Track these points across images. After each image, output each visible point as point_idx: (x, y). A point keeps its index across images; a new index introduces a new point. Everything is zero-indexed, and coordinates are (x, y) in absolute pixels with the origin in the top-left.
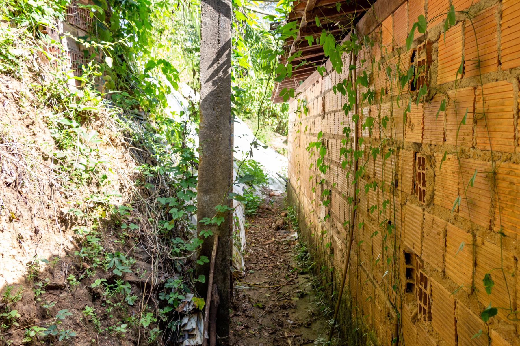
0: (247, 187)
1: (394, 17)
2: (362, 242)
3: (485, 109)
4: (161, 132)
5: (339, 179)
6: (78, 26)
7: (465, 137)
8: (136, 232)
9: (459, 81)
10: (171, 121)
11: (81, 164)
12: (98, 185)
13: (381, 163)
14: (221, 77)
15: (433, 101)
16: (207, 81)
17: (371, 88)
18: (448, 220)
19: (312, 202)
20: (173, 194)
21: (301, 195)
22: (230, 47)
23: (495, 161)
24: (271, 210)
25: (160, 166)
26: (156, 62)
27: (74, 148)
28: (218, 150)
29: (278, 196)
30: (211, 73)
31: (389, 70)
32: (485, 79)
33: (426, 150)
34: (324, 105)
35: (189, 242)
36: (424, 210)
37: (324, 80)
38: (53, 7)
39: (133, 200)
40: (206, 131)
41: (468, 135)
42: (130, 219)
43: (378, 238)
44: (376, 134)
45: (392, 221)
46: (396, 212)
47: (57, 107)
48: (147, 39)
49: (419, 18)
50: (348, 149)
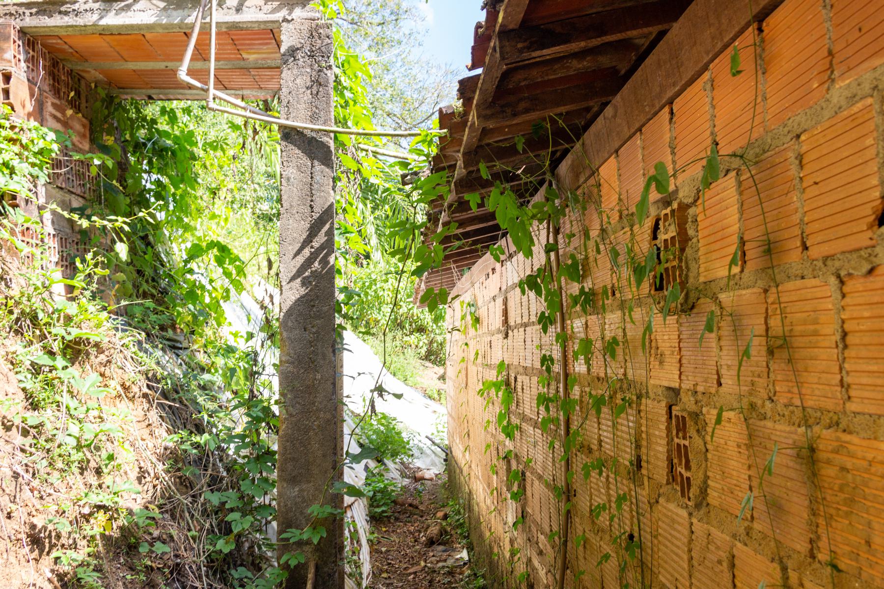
0: (372, 464)
1: (619, 159)
2: (583, 573)
3: (786, 329)
4: (213, 371)
5: (538, 451)
6: (71, 189)
7: (754, 379)
8: (166, 557)
9: (737, 277)
10: (230, 350)
11: (69, 435)
12: (98, 472)
13: (610, 423)
14: (316, 271)
15: (695, 311)
16: (293, 279)
17: (585, 285)
18: (734, 536)
19: (492, 493)
20: (234, 486)
21: (472, 479)
22: (332, 217)
23: (810, 426)
24: (417, 508)
25: (210, 433)
26: (204, 245)
27: (58, 406)
28: (314, 403)
29: (431, 480)
30: (298, 265)
31: (615, 254)
32: (783, 274)
33: (688, 402)
34: (505, 313)
35: (263, 574)
36: (690, 514)
37: (504, 267)
38: (30, 160)
39: (162, 498)
40: (291, 369)
41: (759, 376)
42: (156, 533)
43: (611, 567)
44: (598, 369)
45: (636, 534)
46: (641, 518)
47: (31, 333)
48: (188, 206)
49: (656, 168)
50: (551, 395)
